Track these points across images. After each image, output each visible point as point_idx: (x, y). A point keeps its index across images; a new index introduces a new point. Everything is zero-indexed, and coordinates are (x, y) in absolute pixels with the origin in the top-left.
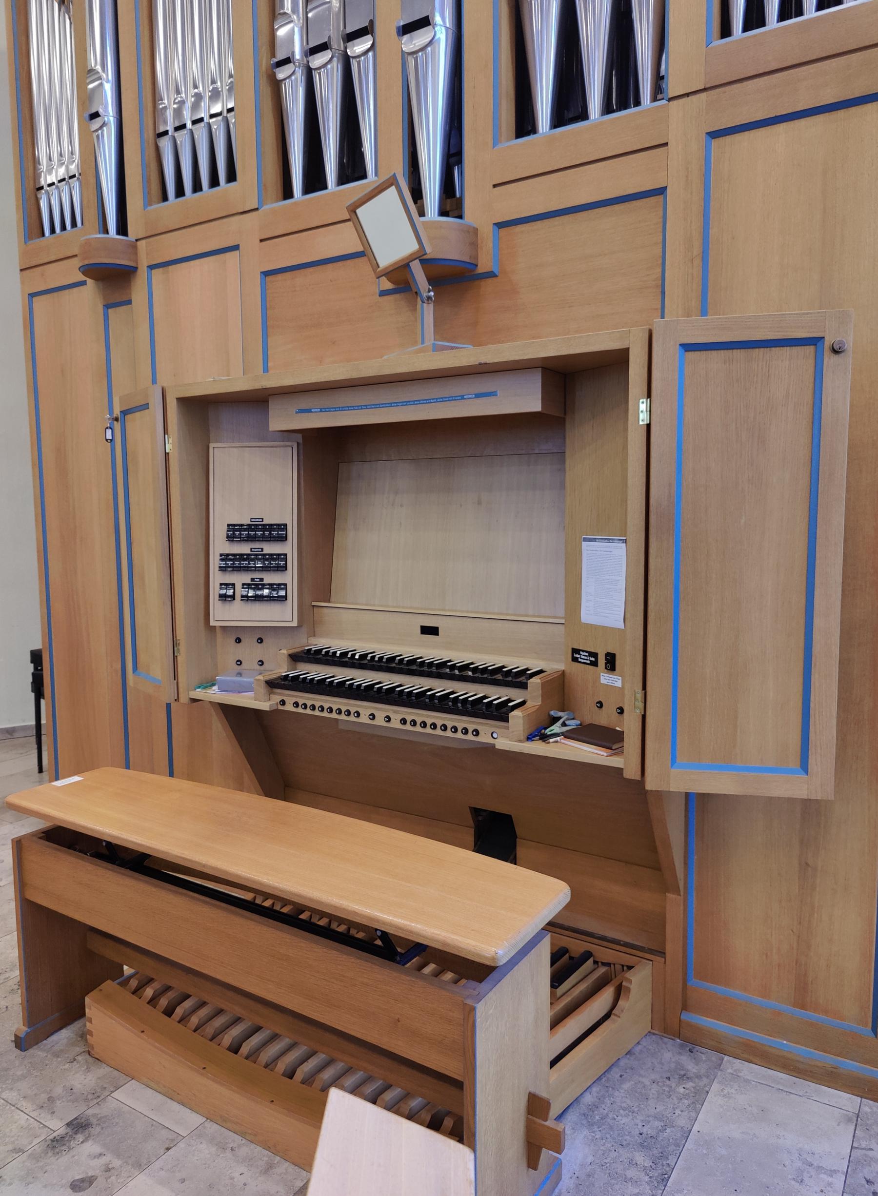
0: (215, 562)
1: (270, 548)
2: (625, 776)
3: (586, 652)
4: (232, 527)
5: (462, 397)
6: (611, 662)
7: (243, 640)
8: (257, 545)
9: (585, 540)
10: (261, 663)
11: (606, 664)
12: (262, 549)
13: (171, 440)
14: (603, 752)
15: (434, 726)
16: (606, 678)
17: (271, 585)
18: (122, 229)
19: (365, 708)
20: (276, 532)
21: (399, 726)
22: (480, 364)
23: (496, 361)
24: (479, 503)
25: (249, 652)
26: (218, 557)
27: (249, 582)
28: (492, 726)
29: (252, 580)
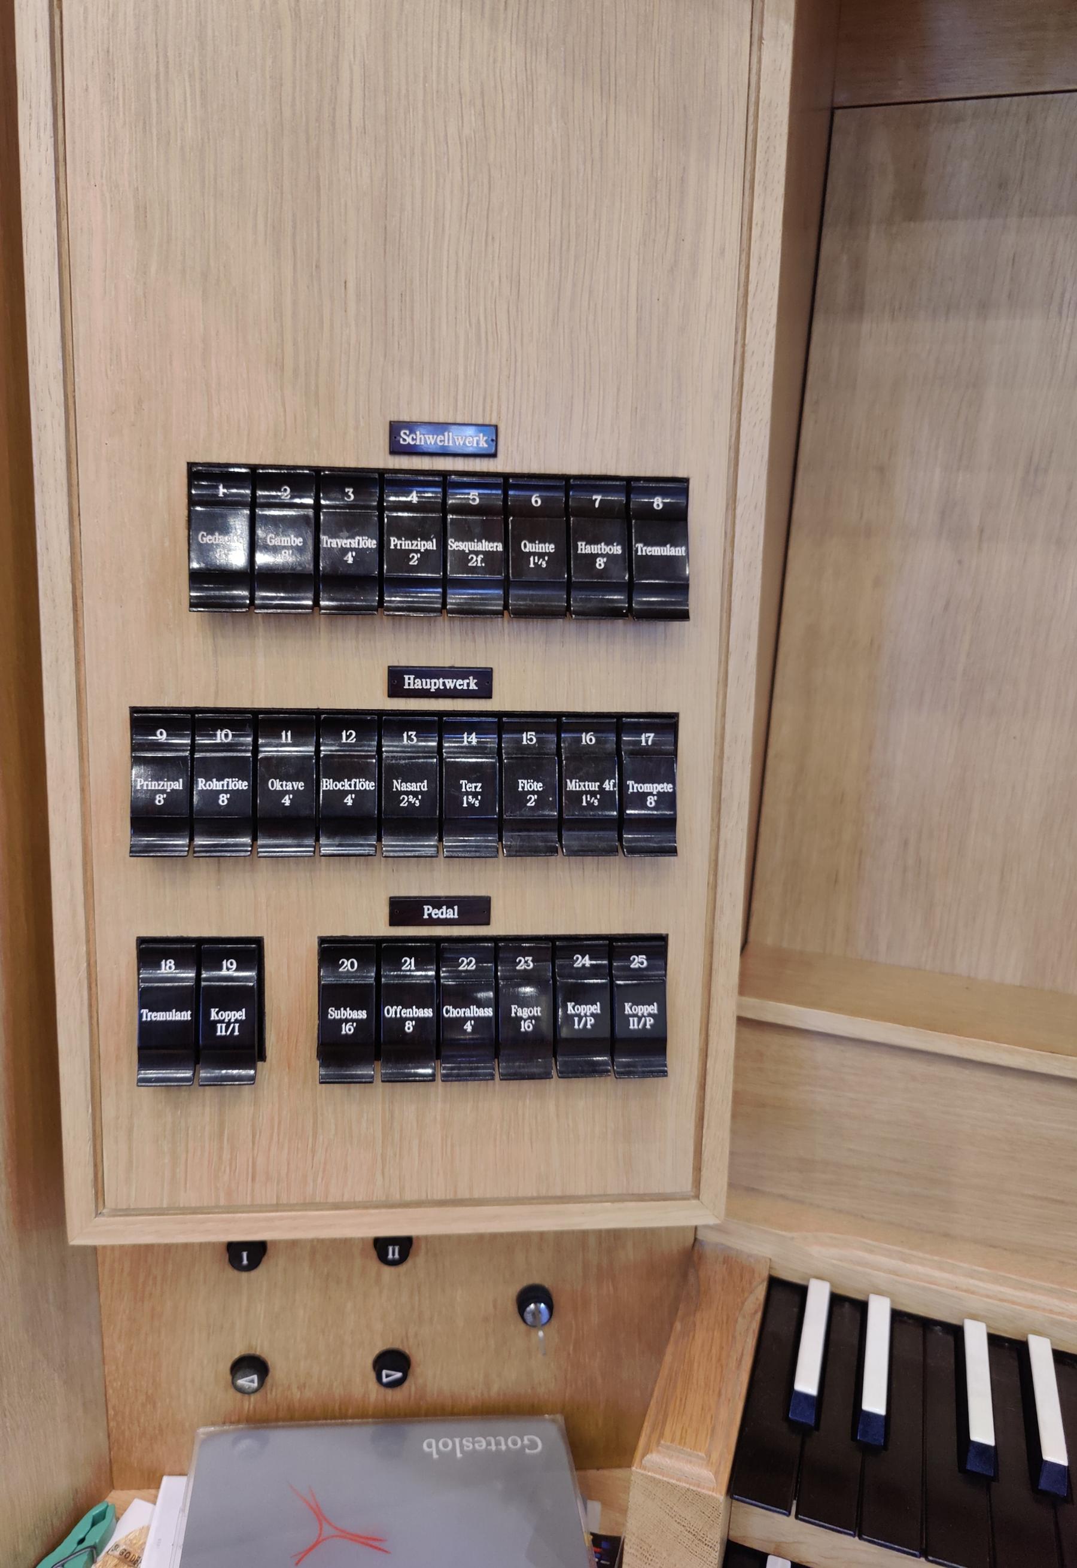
8: (443, 646)
11: (860, 1538)
12: (485, 678)
17: (555, 948)
20: (599, 547)
26: (114, 737)
27: (379, 926)
29: (404, 910)
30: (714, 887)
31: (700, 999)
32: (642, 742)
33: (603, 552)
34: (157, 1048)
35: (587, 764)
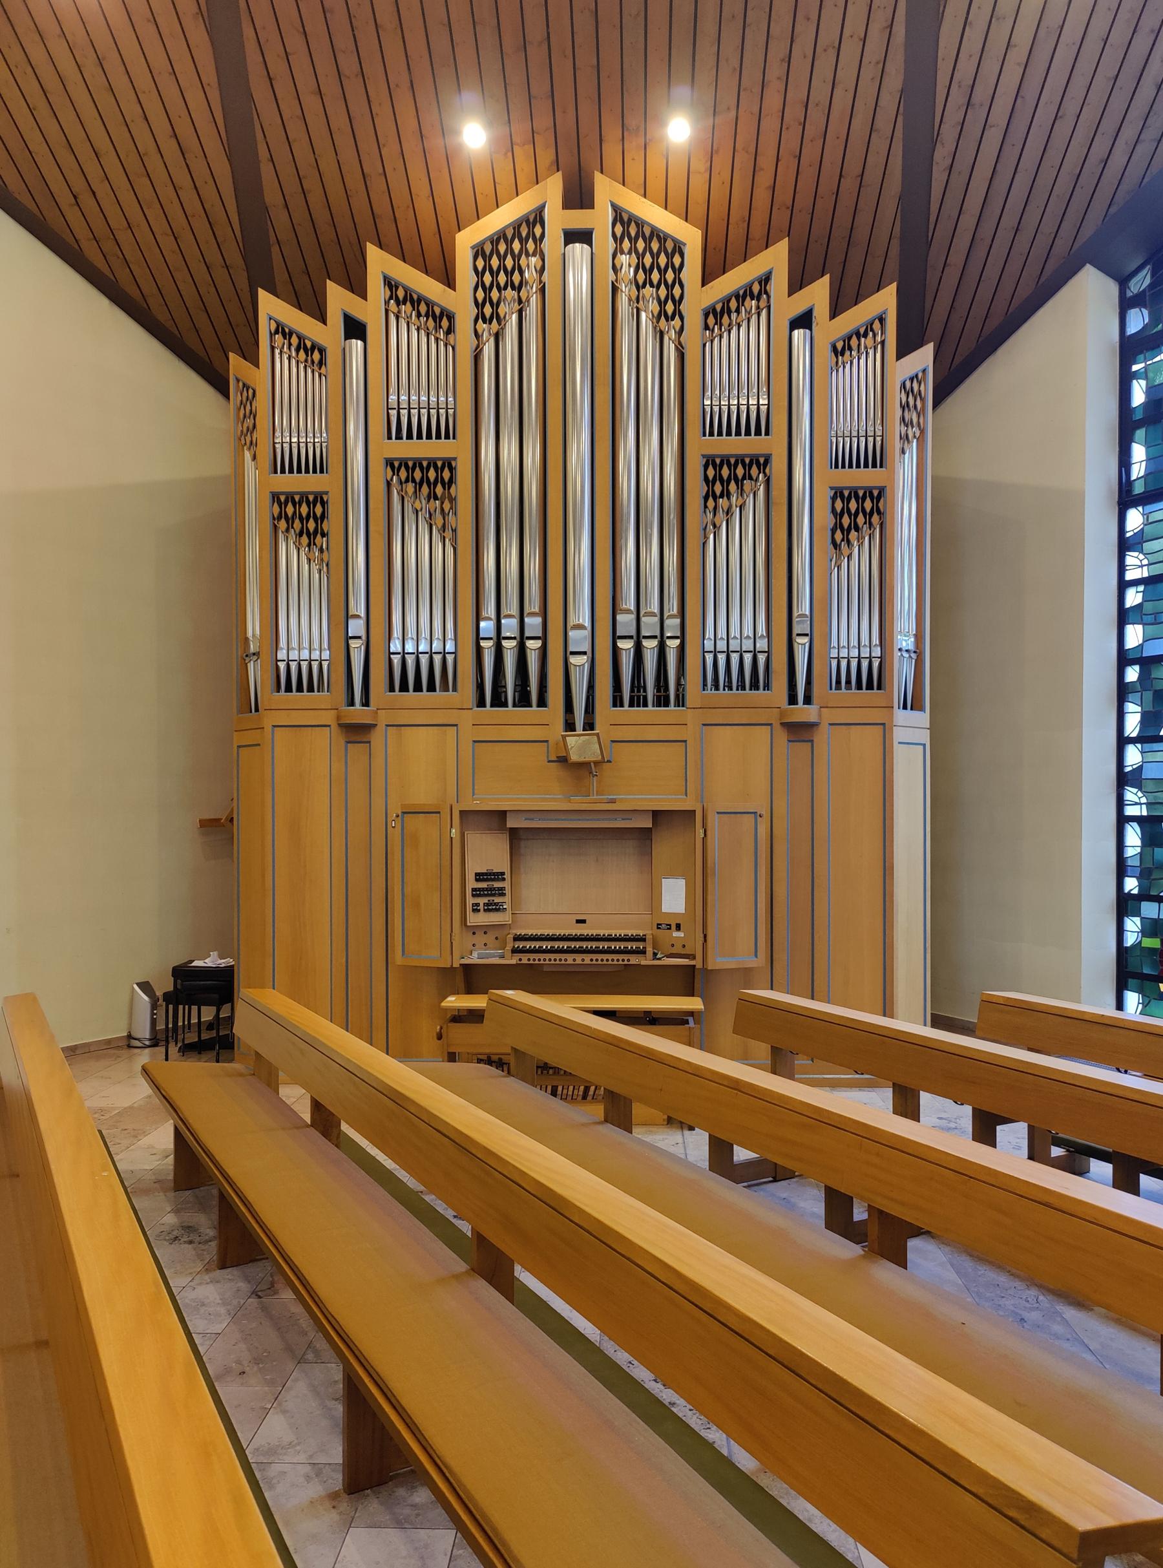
0: (469, 892)
1: (497, 885)
2: (1088, 265)
4: (477, 874)
6: (678, 927)
16: (676, 934)
18: (366, 703)
20: (499, 876)
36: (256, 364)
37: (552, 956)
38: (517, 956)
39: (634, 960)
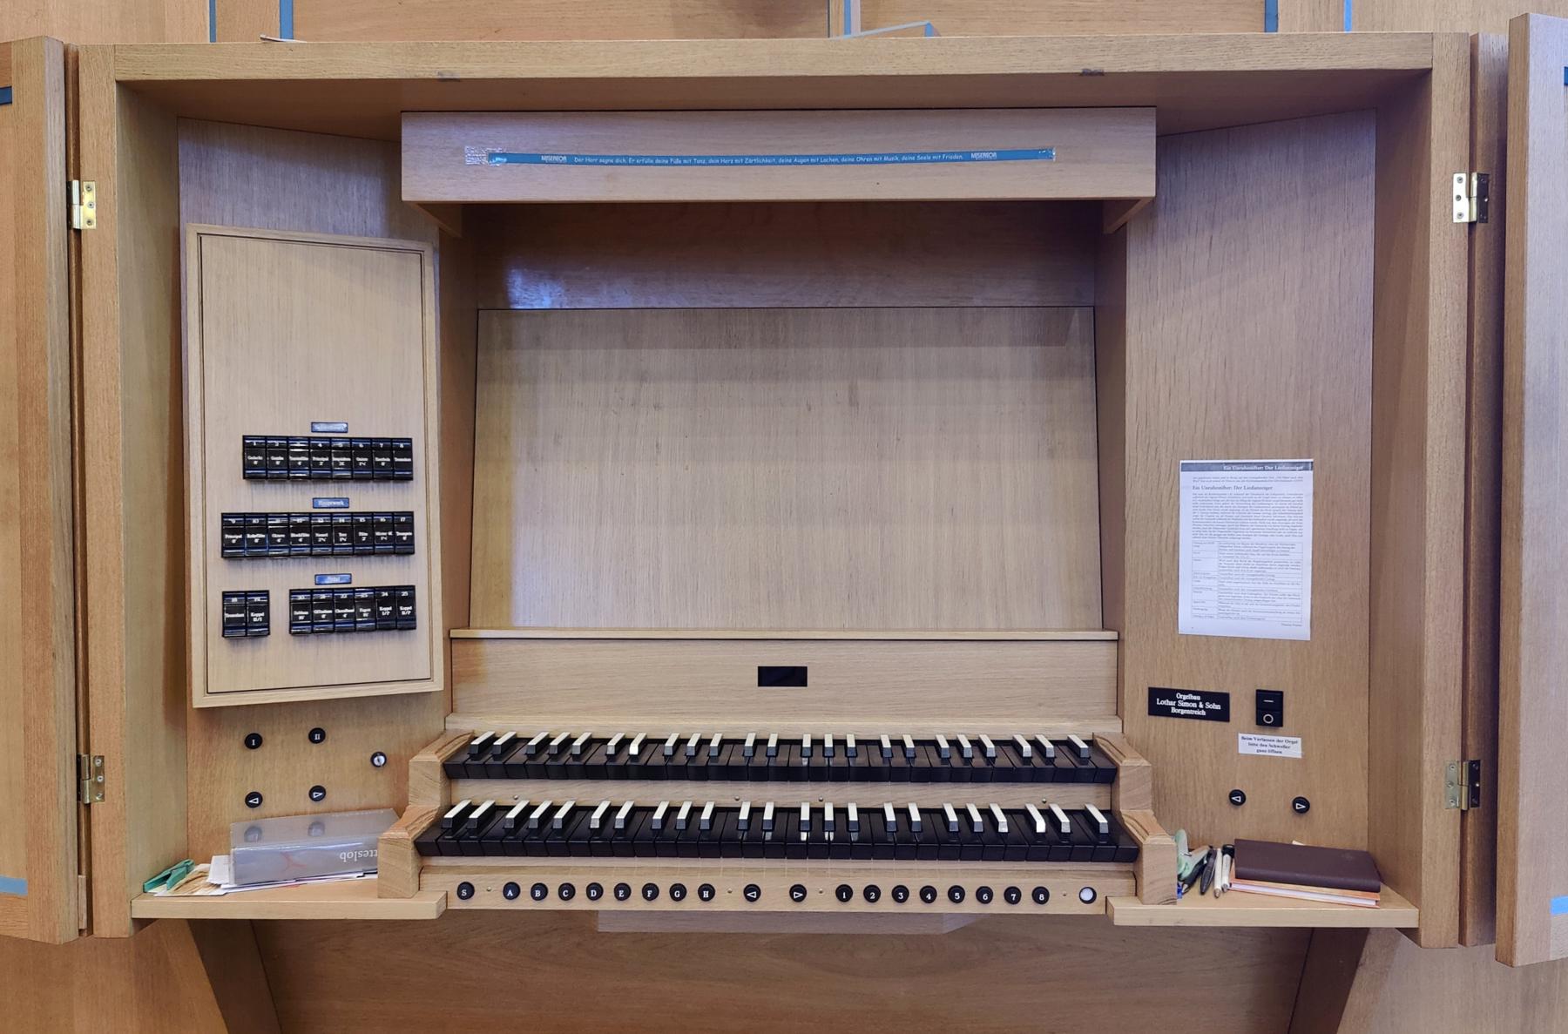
3: (1195, 693)
4: (252, 446)
5: (967, 157)
6: (1270, 710)
7: (266, 737)
9: (1187, 468)
10: (318, 792)
13: (89, 197)
14: (1366, 900)
15: (928, 893)
16: (1252, 743)
19: (728, 878)
20: (385, 459)
21: (834, 906)
22: (1086, 74)
23: (1127, 69)
24: (853, 402)
25: (342, 763)
26: (215, 527)
28: (1083, 874)
30: (429, 569)
31: (430, 608)
32: (402, 521)
33: (384, 460)
34: (229, 628)
35: (382, 527)
36: (1065, 811)
37: (637, 870)
38: (448, 873)
39: (1070, 889)
